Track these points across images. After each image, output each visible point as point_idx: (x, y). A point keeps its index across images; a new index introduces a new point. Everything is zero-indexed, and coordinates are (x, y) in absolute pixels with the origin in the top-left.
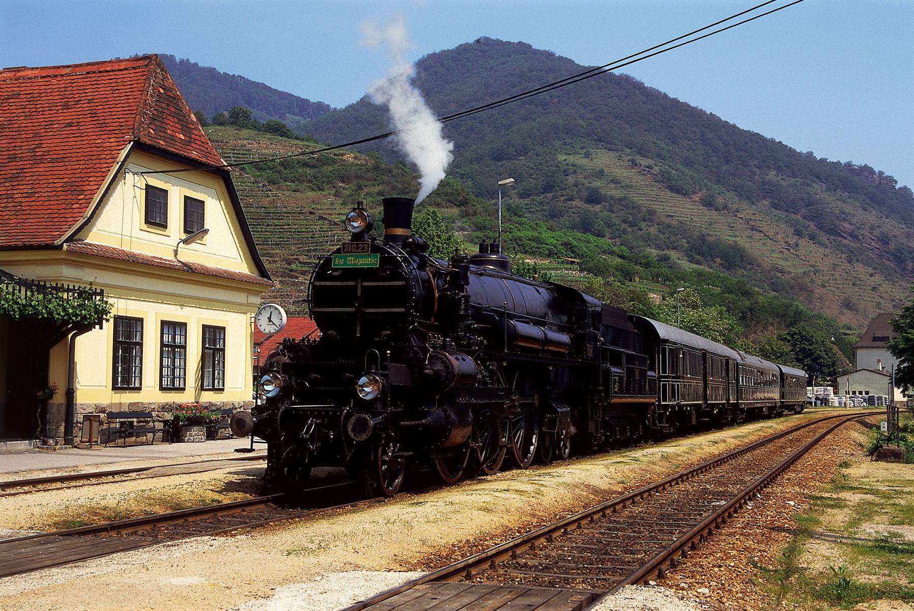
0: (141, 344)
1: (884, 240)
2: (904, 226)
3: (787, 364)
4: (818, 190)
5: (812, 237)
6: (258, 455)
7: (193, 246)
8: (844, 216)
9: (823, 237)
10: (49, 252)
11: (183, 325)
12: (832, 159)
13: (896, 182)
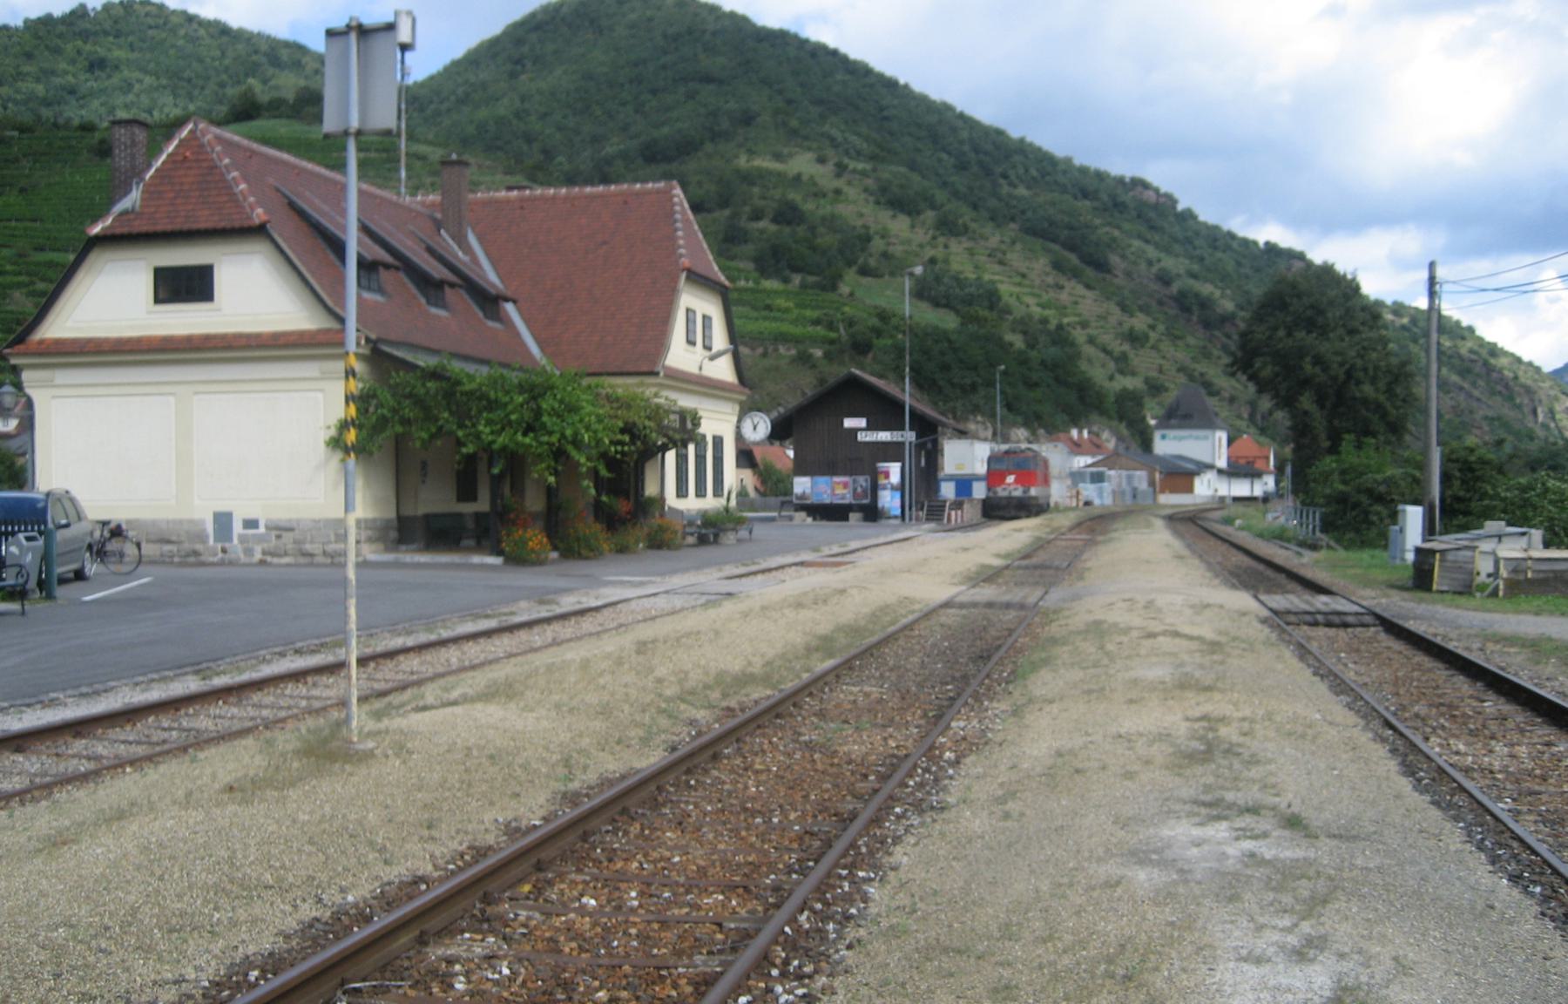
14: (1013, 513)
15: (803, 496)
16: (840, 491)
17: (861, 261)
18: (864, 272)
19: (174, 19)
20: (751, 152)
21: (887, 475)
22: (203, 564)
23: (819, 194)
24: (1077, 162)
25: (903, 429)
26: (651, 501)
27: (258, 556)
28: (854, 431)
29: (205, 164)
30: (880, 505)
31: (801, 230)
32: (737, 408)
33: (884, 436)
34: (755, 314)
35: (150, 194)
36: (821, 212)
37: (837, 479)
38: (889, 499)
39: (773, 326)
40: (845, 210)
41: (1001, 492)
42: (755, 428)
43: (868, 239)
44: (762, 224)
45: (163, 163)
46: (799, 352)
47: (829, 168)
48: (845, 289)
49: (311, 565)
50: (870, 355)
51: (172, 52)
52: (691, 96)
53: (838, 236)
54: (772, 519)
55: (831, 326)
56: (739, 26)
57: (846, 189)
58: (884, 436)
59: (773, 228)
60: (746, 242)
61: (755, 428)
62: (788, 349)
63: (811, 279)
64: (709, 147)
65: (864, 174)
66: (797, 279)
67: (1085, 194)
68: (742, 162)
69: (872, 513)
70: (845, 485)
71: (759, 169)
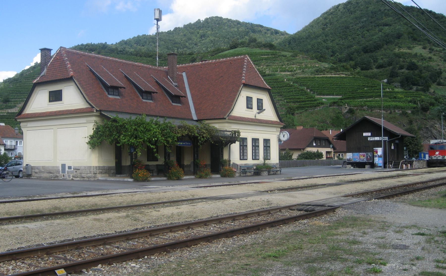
0: (247, 146)
6: (16, 200)
7: (261, 114)
10: (214, 120)
11: (258, 139)
14: (438, 165)
15: (349, 160)
16: (362, 158)
17: (438, 80)
18: (439, 84)
19: (225, 21)
20: (400, 47)
21: (377, 152)
22: (59, 180)
23: (423, 59)
25: (381, 136)
26: (225, 161)
27: (71, 178)
28: (367, 137)
29: (61, 60)
30: (375, 162)
31: (416, 72)
32: (280, 129)
33: (377, 138)
34: (390, 100)
35: (49, 70)
36: (424, 65)
37: (361, 154)
38: (377, 160)
39: (394, 104)
40: (432, 64)
41: (434, 158)
42: (284, 137)
43: (441, 73)
44: (403, 71)
45: (52, 61)
46: (402, 112)
47: (427, 50)
48: (432, 90)
49: (83, 180)
50: (428, 112)
51: (224, 31)
52: (380, 31)
53: (430, 73)
54: (340, 168)
55: (415, 103)
56: (398, 5)
57: (433, 57)
58: (377, 138)
59: (407, 71)
60: (397, 77)
61: (284, 137)
62: (399, 111)
63: (419, 87)
64: (385, 46)
65: (440, 51)
66: (415, 88)
68: (397, 50)
69: (373, 165)
70: (364, 156)
71: (402, 52)
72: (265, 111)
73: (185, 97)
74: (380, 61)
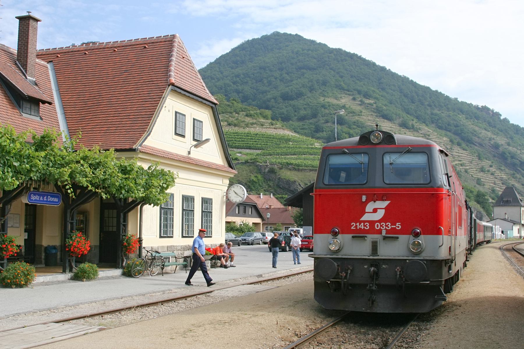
1: (496, 146)
2: (506, 139)
3: (303, 250)
4: (462, 118)
5: (459, 144)
8: (474, 134)
9: (464, 145)
12: (307, 38)
13: (501, 115)
24: (460, 100)
67: (462, 111)
72: (208, 143)
73: (50, 103)
74: (303, 112)
